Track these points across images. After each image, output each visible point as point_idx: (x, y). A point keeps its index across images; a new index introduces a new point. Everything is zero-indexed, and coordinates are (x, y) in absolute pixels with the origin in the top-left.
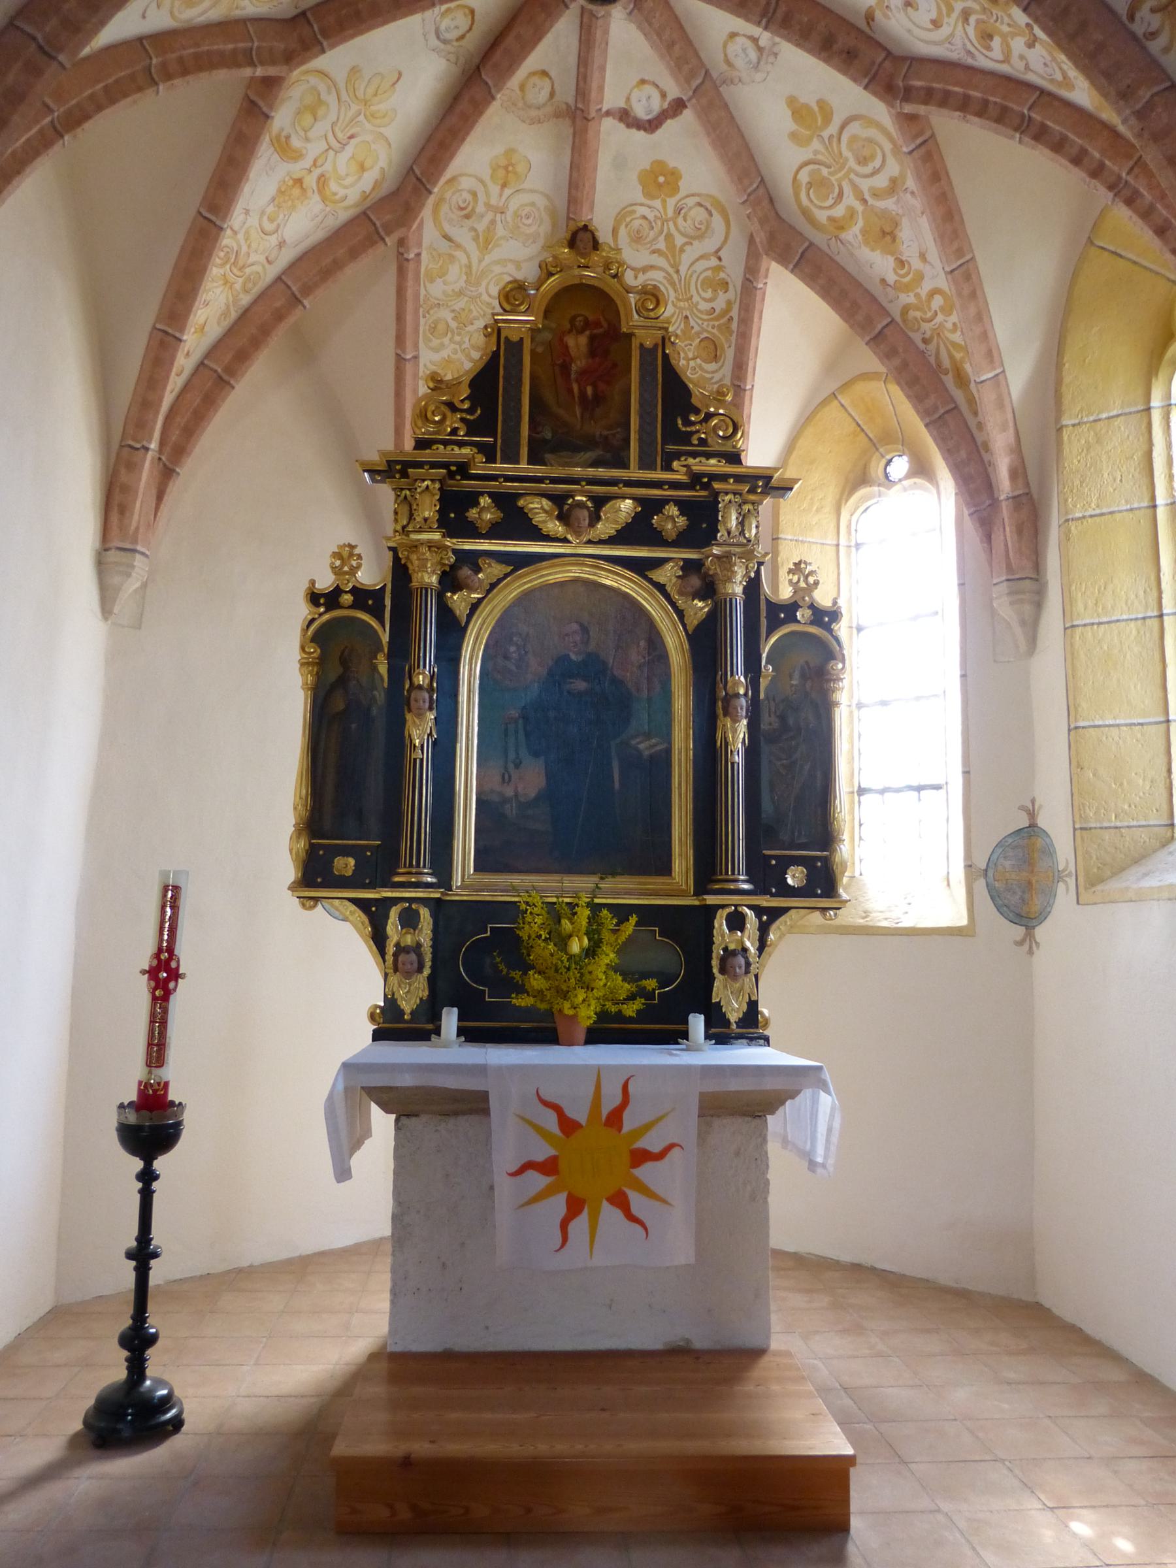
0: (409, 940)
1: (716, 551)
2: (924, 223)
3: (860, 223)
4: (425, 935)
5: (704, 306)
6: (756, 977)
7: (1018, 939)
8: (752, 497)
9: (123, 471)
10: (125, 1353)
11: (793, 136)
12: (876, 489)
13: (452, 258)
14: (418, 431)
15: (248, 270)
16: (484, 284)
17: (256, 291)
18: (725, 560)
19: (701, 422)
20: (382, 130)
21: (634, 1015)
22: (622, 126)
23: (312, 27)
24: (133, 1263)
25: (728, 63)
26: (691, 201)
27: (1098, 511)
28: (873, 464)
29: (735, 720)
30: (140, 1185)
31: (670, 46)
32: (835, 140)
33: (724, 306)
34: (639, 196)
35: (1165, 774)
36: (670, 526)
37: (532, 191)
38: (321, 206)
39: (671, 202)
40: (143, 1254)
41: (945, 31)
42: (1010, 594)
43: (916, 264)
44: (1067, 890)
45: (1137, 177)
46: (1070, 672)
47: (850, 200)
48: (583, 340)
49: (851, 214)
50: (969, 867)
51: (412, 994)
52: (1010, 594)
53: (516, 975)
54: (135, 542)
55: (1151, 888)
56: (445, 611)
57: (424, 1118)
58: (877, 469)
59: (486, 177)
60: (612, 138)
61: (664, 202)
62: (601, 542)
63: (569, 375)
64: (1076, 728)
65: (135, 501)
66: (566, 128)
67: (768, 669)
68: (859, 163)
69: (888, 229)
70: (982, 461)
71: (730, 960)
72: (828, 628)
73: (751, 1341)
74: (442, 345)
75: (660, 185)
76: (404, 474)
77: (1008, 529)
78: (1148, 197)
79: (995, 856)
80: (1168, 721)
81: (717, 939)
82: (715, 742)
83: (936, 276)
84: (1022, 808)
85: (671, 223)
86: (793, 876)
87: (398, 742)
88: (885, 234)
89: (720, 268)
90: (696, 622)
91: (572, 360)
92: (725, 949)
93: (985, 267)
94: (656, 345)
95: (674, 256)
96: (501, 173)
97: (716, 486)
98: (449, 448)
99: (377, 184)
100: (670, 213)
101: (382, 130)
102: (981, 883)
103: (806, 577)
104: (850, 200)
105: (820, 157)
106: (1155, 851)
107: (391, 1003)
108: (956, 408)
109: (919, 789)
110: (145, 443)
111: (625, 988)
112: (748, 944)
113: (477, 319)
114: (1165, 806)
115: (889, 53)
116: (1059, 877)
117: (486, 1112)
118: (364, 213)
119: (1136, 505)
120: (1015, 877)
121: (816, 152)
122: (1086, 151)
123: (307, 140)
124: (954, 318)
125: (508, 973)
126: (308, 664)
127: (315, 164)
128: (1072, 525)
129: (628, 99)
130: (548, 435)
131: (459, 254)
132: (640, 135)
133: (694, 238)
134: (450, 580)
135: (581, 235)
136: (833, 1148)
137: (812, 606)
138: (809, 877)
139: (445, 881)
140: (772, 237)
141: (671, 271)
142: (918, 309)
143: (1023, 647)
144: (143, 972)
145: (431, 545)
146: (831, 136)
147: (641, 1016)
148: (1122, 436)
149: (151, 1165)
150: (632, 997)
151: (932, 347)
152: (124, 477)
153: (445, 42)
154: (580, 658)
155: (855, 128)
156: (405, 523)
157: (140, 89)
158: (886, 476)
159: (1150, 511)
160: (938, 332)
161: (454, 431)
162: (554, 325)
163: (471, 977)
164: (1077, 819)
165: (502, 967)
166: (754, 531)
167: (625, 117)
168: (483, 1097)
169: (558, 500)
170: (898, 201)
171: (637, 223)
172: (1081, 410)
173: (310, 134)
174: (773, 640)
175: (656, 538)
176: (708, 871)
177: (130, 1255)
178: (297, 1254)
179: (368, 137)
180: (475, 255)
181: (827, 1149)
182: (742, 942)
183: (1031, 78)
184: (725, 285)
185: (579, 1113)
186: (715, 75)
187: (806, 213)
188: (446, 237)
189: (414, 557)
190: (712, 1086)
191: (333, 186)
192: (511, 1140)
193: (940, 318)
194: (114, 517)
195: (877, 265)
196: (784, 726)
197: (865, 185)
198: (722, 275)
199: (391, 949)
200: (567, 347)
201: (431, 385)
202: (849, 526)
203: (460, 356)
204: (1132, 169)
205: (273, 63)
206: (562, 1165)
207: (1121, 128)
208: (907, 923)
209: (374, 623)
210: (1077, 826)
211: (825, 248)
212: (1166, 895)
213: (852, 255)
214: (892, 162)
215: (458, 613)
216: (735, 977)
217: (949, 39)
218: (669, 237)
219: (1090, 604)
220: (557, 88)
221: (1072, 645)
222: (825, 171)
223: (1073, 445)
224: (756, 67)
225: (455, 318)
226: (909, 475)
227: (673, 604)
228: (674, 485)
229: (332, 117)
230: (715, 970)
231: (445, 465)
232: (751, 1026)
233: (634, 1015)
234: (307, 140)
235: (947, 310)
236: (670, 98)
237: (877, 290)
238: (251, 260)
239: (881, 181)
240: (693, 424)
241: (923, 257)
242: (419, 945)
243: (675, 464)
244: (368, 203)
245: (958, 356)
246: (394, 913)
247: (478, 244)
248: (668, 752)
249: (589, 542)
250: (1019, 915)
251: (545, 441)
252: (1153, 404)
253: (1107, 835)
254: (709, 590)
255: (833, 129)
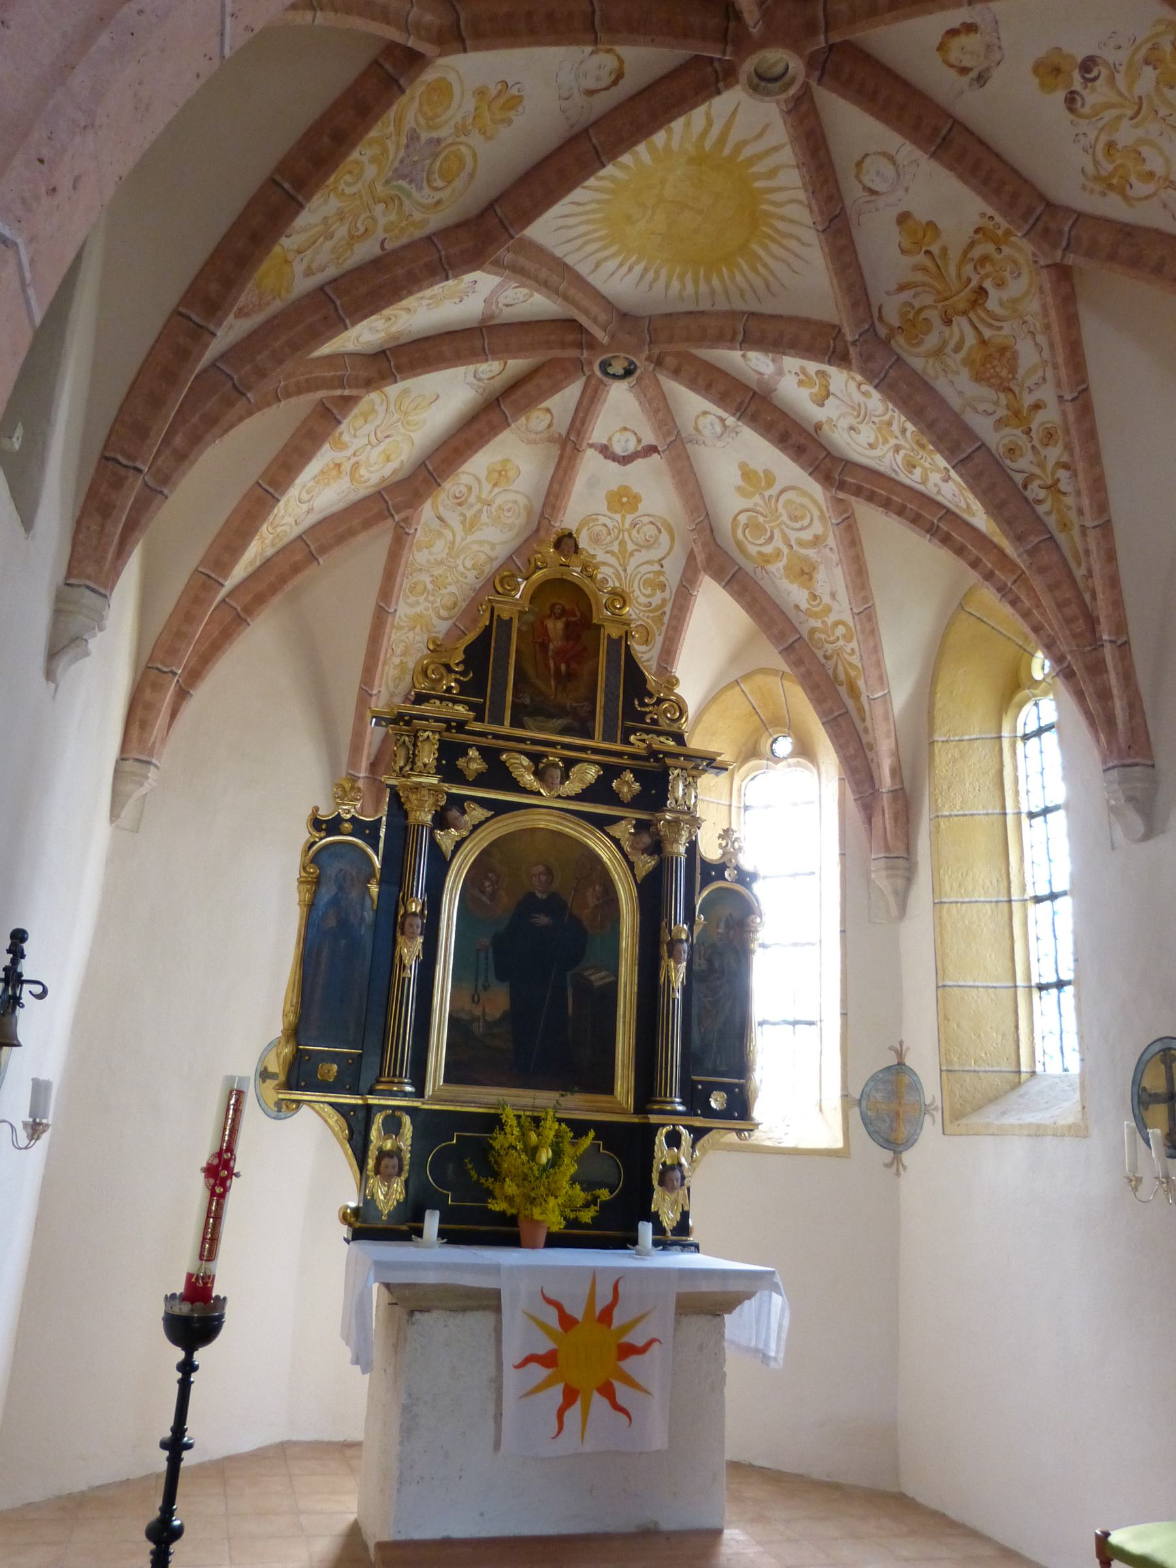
0: (388, 1145)
1: (668, 816)
2: (838, 572)
3: (785, 561)
4: (406, 1138)
5: (642, 600)
6: (689, 1190)
7: (888, 1161)
8: (694, 773)
9: (148, 691)
10: (152, 1546)
11: (739, 489)
12: (765, 762)
13: (440, 534)
14: (417, 685)
15: (279, 530)
16: (462, 557)
17: (280, 545)
18: (676, 823)
19: (653, 705)
20: (411, 434)
21: (589, 1221)
22: (601, 457)
23: (389, 361)
24: (166, 1453)
25: (697, 429)
26: (646, 520)
27: (961, 812)
28: (762, 741)
29: (678, 962)
30: (180, 1375)
31: (657, 411)
32: (773, 500)
33: (660, 602)
34: (603, 507)
35: (1013, 1029)
36: (625, 789)
37: (517, 492)
38: (348, 484)
39: (629, 518)
40: (176, 1445)
41: (877, 453)
42: (887, 869)
43: (827, 599)
44: (934, 1121)
45: (1019, 587)
46: (939, 941)
47: (778, 542)
48: (560, 625)
49: (778, 554)
50: (845, 1096)
51: (389, 1195)
52: (887, 869)
53: (489, 1183)
54: (151, 755)
55: (1012, 1125)
56: (434, 846)
57: (435, 1314)
58: (765, 747)
59: (482, 477)
60: (590, 463)
61: (623, 517)
62: (569, 798)
63: (547, 652)
64: (944, 986)
65: (156, 718)
66: (555, 451)
67: (700, 918)
68: (791, 519)
69: (806, 570)
70: (866, 757)
71: (670, 1174)
72: (748, 885)
73: (706, 1522)
74: (418, 603)
75: (623, 504)
76: (408, 723)
77: (887, 816)
78: (1027, 604)
79: (868, 1089)
80: (1016, 987)
81: (657, 1154)
82: (659, 979)
83: (842, 610)
84: (891, 1048)
85: (626, 534)
86: (716, 1100)
87: (390, 960)
88: (805, 573)
89: (660, 573)
90: (644, 873)
91: (550, 640)
92: (664, 1164)
93: (881, 612)
94: (621, 638)
95: (624, 558)
96: (496, 475)
97: (668, 761)
98: (444, 703)
99: (395, 472)
100: (627, 525)
101: (411, 434)
102: (855, 1113)
103: (733, 843)
104: (778, 542)
105: (758, 508)
106: (1006, 1093)
107: (368, 1203)
108: (847, 712)
109: (795, 1023)
110: (174, 669)
111: (580, 1196)
112: (683, 1161)
113: (450, 584)
114: (1013, 1056)
115: (829, 453)
116: (926, 1110)
117: (498, 1309)
118: (379, 492)
119: (990, 811)
120: (885, 1106)
121: (756, 504)
122: (981, 561)
123: (355, 436)
124: (854, 644)
125: (478, 1179)
126: (308, 882)
127: (354, 455)
128: (942, 822)
129: (610, 439)
130: (527, 701)
131: (448, 535)
132: (613, 466)
133: (644, 547)
134: (441, 821)
135: (565, 539)
136: (783, 1343)
137: (737, 868)
138: (728, 1101)
139: (420, 1093)
140: (710, 559)
141: (620, 569)
142: (822, 631)
143: (894, 911)
144: (237, 1175)
145: (431, 788)
146: (770, 496)
147: (596, 1222)
148: (979, 756)
149: (192, 1356)
150: (587, 1205)
151: (831, 663)
152: (148, 695)
153: (479, 380)
154: (545, 897)
155: (790, 495)
156: (402, 764)
157: (269, 405)
158: (773, 753)
159: (1001, 817)
160: (838, 653)
161: (449, 689)
162: (536, 609)
163: (448, 1188)
164: (944, 1061)
165: (473, 1173)
166: (693, 801)
167: (605, 451)
168: (497, 1294)
169: (535, 758)
170: (819, 552)
171: (597, 528)
172: (949, 731)
173: (358, 433)
174: (705, 894)
175: (613, 799)
176: (647, 1091)
177: (164, 1445)
178: (206, 1459)
179: (399, 438)
180: (460, 533)
181: (778, 1345)
182: (678, 1159)
183: (940, 498)
184: (663, 587)
185: (576, 1310)
186: (684, 435)
187: (739, 544)
188: (440, 518)
189: (413, 797)
190: (687, 1287)
191: (362, 471)
192: (520, 1336)
193: (841, 643)
194: (135, 732)
195: (795, 594)
196: (711, 969)
197: (793, 536)
198: (662, 579)
199: (373, 1152)
200: (546, 629)
201: (431, 647)
202: (739, 791)
203: (430, 612)
204: (1015, 582)
205: (357, 386)
206: (561, 1359)
207: (1018, 561)
208: (788, 1143)
209: (370, 851)
210: (944, 1068)
211: (752, 574)
212: (1026, 1132)
213: (773, 582)
214: (817, 523)
215: (444, 848)
216: (672, 1189)
217: (880, 458)
218: (622, 544)
219: (955, 886)
220: (555, 421)
221: (940, 918)
222: (761, 519)
223: (943, 758)
224: (720, 437)
225: (432, 582)
226: (793, 754)
227: (625, 855)
228: (632, 756)
229: (378, 422)
230: (655, 1183)
231: (447, 721)
232: (679, 1235)
233: (589, 1221)
234: (355, 436)
235: (848, 638)
236: (644, 443)
237: (792, 614)
238: (285, 521)
239: (807, 536)
240: (647, 705)
241: (833, 595)
242: (400, 1150)
243: (632, 738)
244: (383, 485)
245: (853, 673)
246: (379, 1119)
247: (464, 526)
248: (615, 983)
249: (559, 797)
250: (888, 1141)
251: (525, 706)
252: (1003, 734)
253: (967, 1077)
254: (657, 847)
255: (773, 491)
